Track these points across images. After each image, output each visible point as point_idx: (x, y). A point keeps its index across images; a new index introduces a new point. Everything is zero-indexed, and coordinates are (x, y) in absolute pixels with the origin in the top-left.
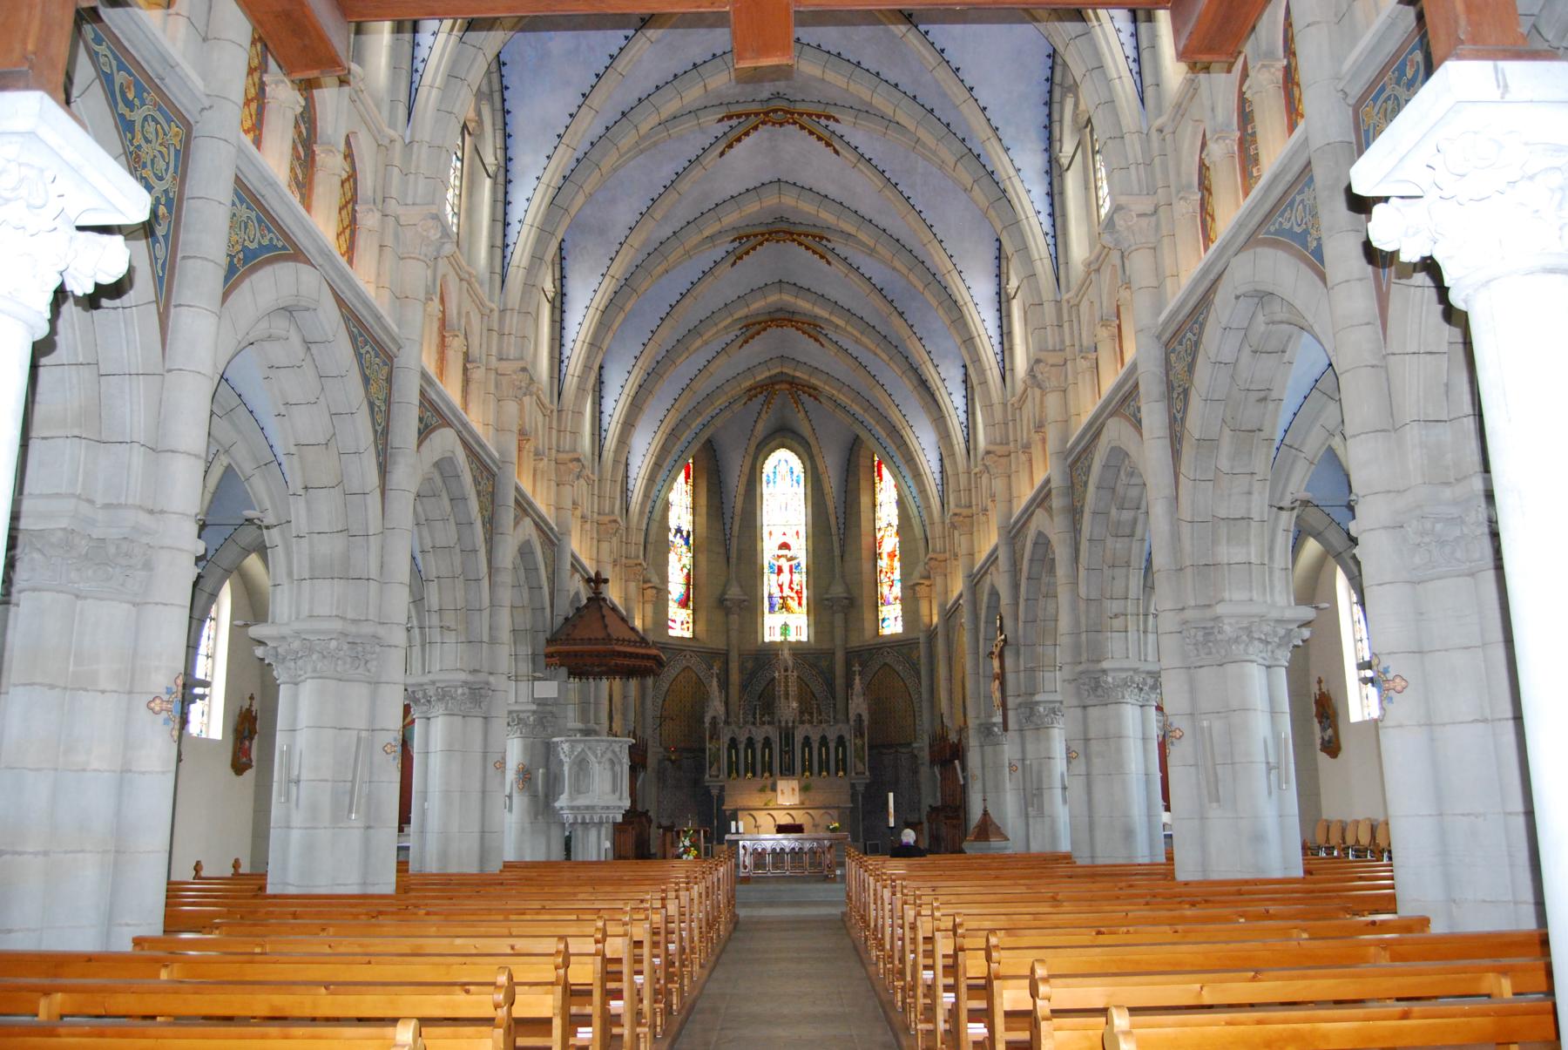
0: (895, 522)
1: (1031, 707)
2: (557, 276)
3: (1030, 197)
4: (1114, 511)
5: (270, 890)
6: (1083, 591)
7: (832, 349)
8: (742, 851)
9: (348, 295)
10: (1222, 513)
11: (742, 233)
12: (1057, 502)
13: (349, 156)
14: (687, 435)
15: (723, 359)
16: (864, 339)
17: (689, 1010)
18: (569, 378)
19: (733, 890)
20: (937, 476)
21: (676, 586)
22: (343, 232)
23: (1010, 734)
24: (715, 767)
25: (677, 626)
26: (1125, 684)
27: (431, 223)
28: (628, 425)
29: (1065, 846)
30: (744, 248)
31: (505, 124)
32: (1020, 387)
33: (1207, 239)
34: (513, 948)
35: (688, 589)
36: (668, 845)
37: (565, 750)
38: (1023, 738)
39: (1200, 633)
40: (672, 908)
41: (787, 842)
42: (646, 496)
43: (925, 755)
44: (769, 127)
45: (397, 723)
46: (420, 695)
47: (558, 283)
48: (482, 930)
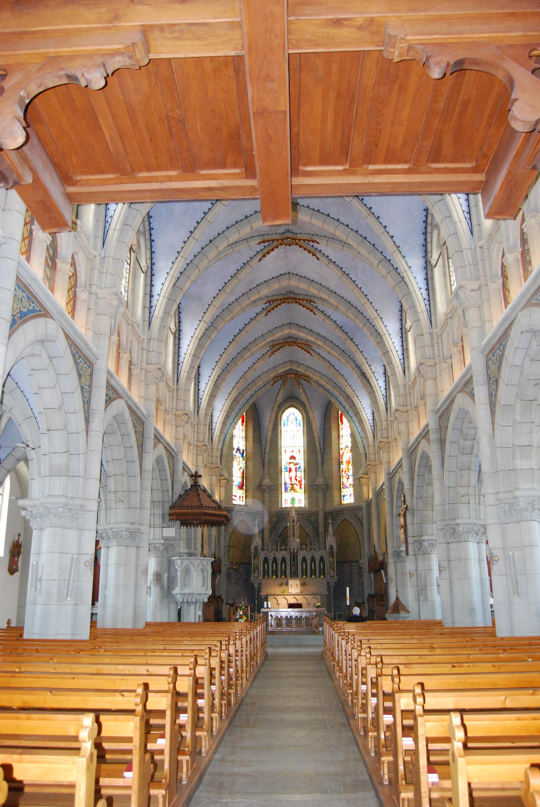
0: (350, 445)
1: (420, 543)
2: (177, 321)
3: (416, 280)
4: (462, 441)
5: (25, 636)
6: (446, 483)
7: (317, 357)
8: (270, 618)
9: (71, 334)
10: (517, 443)
11: (270, 299)
12: (433, 436)
13: (73, 264)
14: (242, 401)
15: (261, 363)
16: (333, 352)
17: (240, 704)
18: (182, 373)
19: (265, 638)
20: (371, 421)
21: (237, 479)
22: (70, 302)
23: (410, 557)
24: (256, 572)
25: (237, 499)
26: (469, 532)
27: (114, 297)
28: (213, 396)
29: (439, 617)
30: (271, 307)
31: (152, 247)
32: (412, 377)
33: (506, 302)
34: (148, 671)
35: (243, 480)
36: (232, 614)
37: (178, 563)
38: (416, 559)
39: (507, 506)
40: (232, 650)
41: (294, 613)
42: (222, 432)
43: (366, 567)
44: (283, 246)
45: (91, 550)
46: (104, 535)
47: (177, 325)
48: (133, 660)
